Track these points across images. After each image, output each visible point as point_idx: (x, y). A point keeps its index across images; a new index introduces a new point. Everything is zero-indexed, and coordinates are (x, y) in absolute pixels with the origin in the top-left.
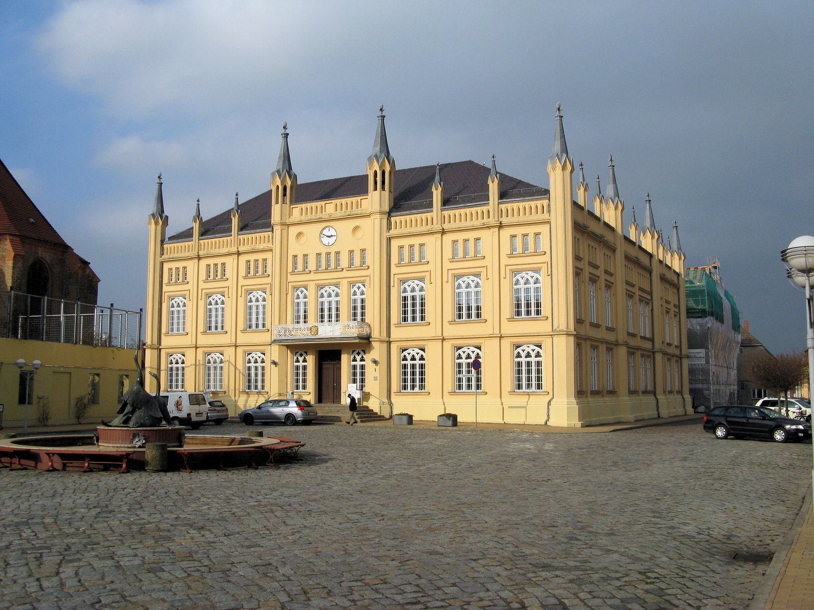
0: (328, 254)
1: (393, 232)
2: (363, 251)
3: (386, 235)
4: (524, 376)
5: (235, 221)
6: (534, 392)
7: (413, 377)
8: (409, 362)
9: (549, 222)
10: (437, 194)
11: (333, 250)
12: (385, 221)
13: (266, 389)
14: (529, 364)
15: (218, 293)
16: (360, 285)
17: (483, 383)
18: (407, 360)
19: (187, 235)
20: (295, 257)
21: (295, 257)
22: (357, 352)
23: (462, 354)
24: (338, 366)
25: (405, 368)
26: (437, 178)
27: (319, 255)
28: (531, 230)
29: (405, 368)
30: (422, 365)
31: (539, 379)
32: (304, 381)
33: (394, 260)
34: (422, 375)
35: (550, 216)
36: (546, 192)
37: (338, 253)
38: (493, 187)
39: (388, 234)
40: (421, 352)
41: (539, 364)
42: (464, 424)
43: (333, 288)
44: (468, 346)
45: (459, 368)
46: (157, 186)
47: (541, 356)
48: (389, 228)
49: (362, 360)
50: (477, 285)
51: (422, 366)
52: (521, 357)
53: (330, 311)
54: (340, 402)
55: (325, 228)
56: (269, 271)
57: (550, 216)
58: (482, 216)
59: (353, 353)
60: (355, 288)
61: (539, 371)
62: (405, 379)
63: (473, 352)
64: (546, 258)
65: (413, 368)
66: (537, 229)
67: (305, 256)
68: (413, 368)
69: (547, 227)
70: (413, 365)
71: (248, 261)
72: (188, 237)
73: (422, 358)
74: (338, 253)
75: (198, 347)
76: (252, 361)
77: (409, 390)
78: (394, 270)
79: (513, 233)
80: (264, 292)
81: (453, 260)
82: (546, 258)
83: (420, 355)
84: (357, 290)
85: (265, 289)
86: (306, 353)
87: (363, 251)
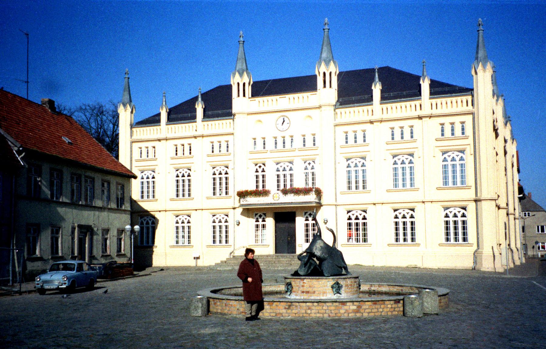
1: (135, 137)
5: (200, 108)
8: (353, 221)
10: (377, 89)
11: (287, 135)
16: (311, 162)
17: (417, 237)
22: (259, 215)
24: (291, 225)
26: (200, 99)
30: (364, 223)
36: (469, 91)
38: (425, 86)
39: (335, 122)
40: (188, 218)
43: (359, 160)
44: (404, 209)
45: (350, 226)
48: (131, 136)
49: (264, 221)
51: (364, 224)
54: (295, 252)
59: (305, 214)
60: (307, 164)
62: (350, 234)
69: (471, 117)
71: (392, 129)
72: (368, 102)
73: (364, 218)
75: (480, 200)
77: (354, 242)
78: (339, 150)
84: (308, 166)
86: (265, 214)
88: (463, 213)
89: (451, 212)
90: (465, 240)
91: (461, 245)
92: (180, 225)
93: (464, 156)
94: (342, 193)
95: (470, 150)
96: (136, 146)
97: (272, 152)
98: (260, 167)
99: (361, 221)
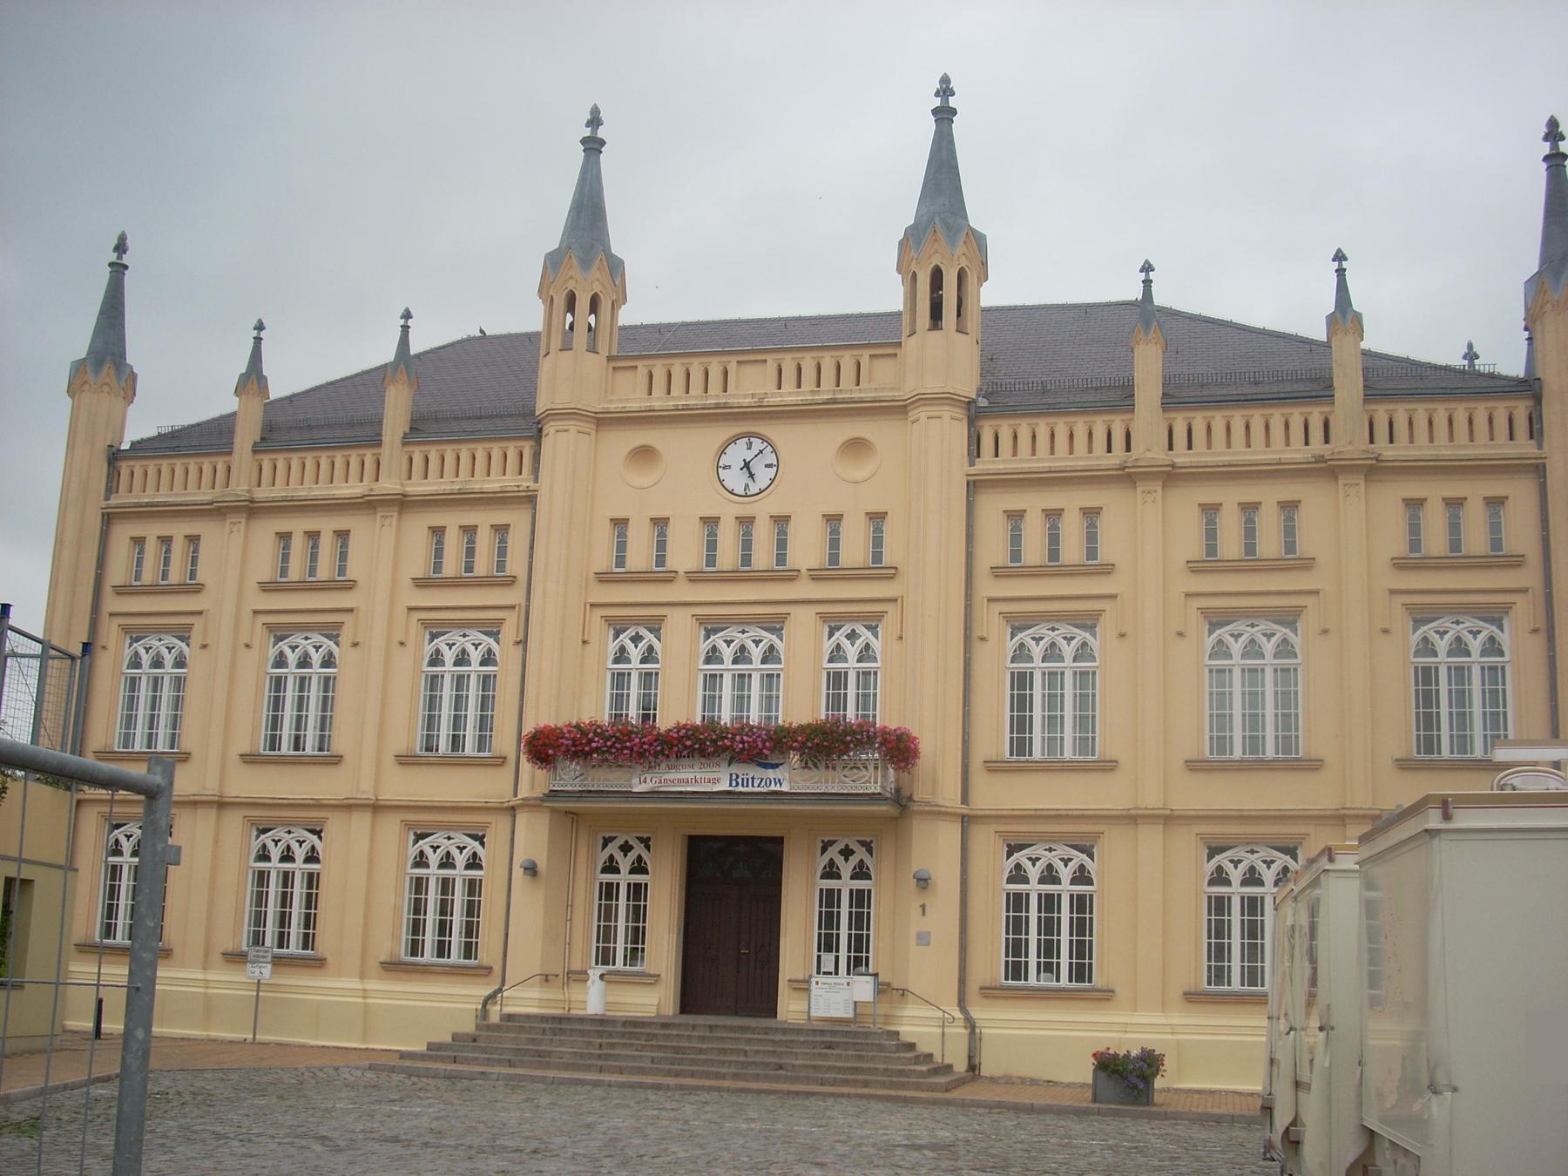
0: (746, 522)
2: (877, 518)
3: (103, 504)
4: (458, 919)
6: (618, 973)
7: (1053, 943)
9: (1539, 470)
11: (763, 510)
12: (960, 432)
13: (488, 952)
14: (1049, 903)
15: (638, 621)
18: (1056, 880)
19: (208, 439)
20: (620, 524)
21: (620, 524)
23: (429, 851)
25: (1018, 908)
27: (711, 523)
28: (484, 519)
29: (1018, 908)
31: (470, 930)
32: (637, 935)
33: (993, 549)
34: (859, 927)
35: (1540, 446)
37: (781, 521)
39: (973, 470)
41: (473, 887)
42: (1042, 1098)
46: (105, 274)
47: (1089, 882)
48: (111, 489)
50: (328, 662)
52: (1228, 883)
53: (300, 709)
55: (734, 440)
56: (516, 564)
57: (1540, 446)
58: (469, 466)
59: (605, 846)
60: (625, 638)
61: (471, 909)
63: (461, 849)
64: (514, 596)
65: (1049, 909)
66: (501, 516)
67: (660, 523)
68: (1049, 909)
70: (1049, 897)
73: (312, 857)
74: (781, 521)
76: (275, 853)
78: (987, 587)
79: (138, 533)
80: (182, 639)
81: (1013, 569)
82: (1529, 577)
83: (1072, 865)
84: (630, 645)
85: (339, 625)
87: (877, 518)
88: (1082, 867)
89: (1236, 863)
90: (469, 950)
91: (425, 971)
92: (1034, 888)
93: (1504, 638)
94: (994, 767)
95: (1525, 612)
96: (992, 507)
97: (694, 578)
98: (626, 848)
99: (1065, 889)
